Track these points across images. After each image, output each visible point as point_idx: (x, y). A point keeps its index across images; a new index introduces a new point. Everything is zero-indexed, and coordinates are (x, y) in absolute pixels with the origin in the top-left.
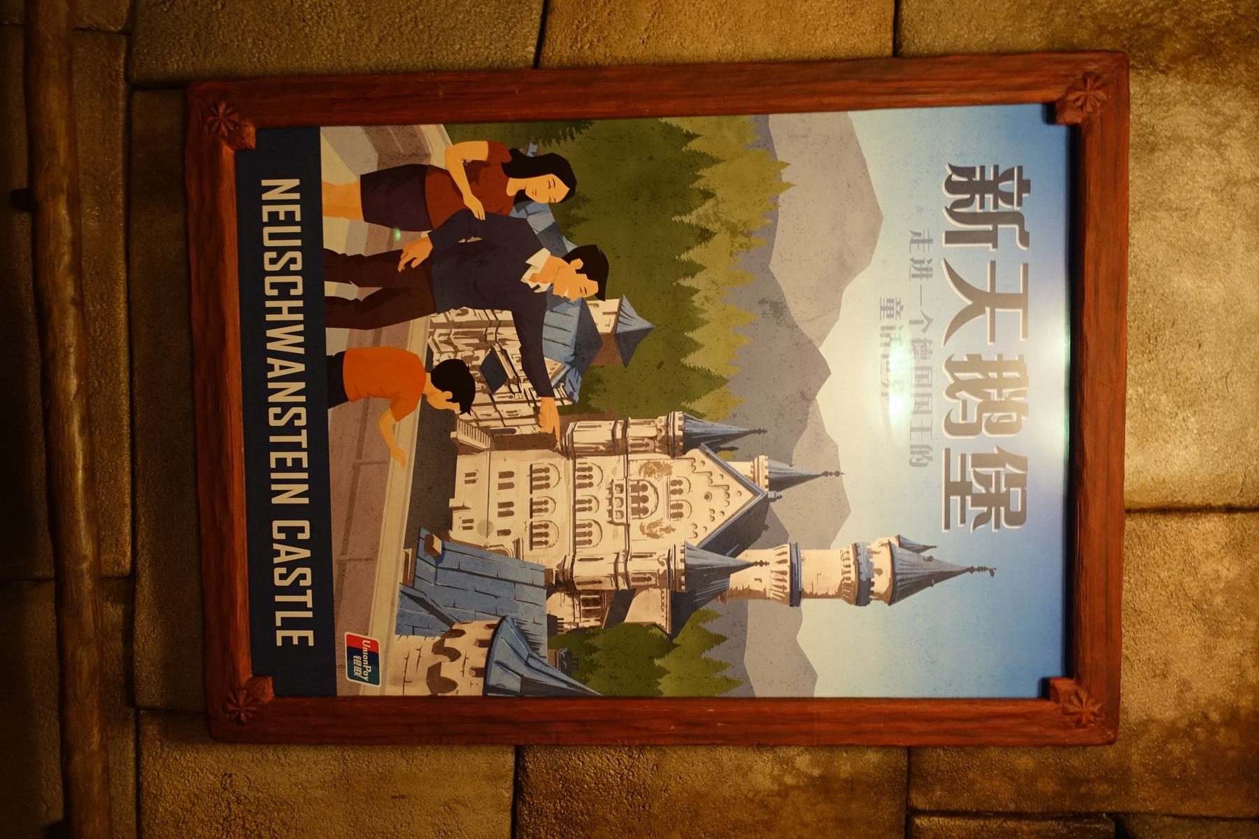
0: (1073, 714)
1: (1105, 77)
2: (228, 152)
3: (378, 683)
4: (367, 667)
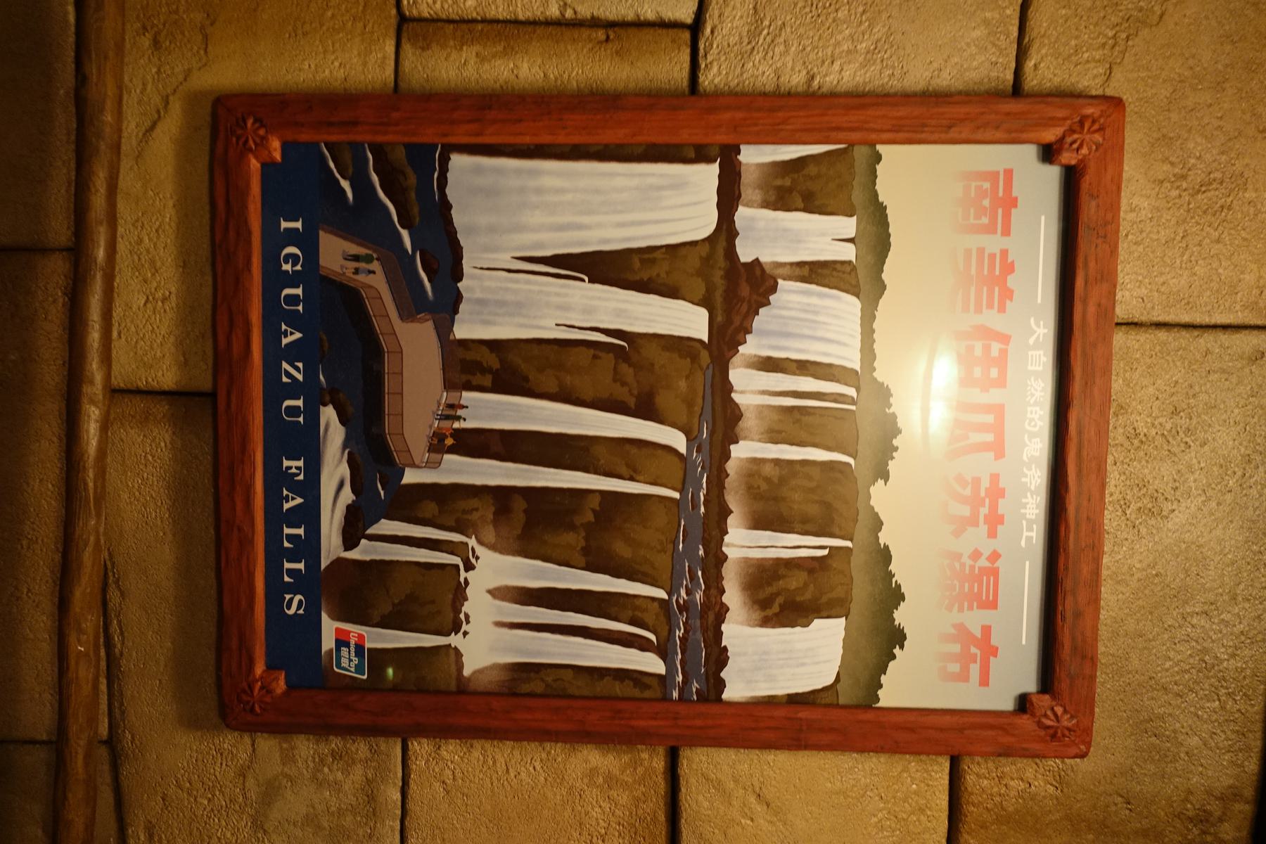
0: (1049, 727)
1: (1102, 121)
2: (255, 164)
4: (354, 659)
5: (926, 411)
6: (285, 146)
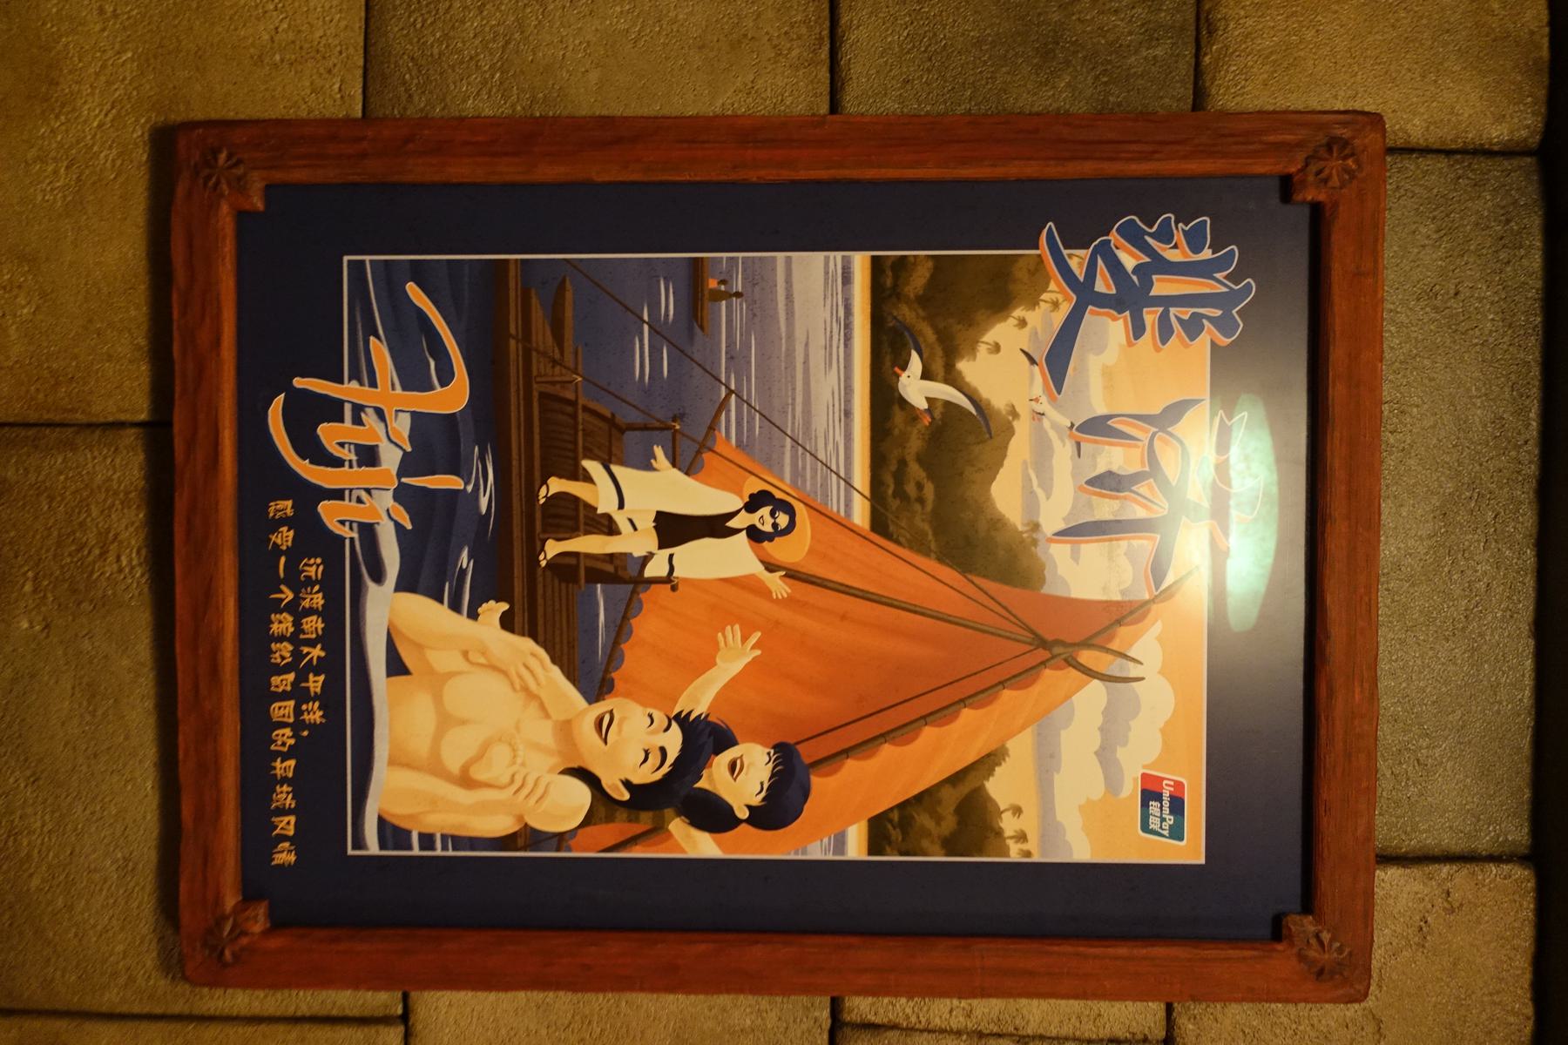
3: (1181, 839)
4: (1168, 817)
5: (1219, 556)
6: (270, 190)
